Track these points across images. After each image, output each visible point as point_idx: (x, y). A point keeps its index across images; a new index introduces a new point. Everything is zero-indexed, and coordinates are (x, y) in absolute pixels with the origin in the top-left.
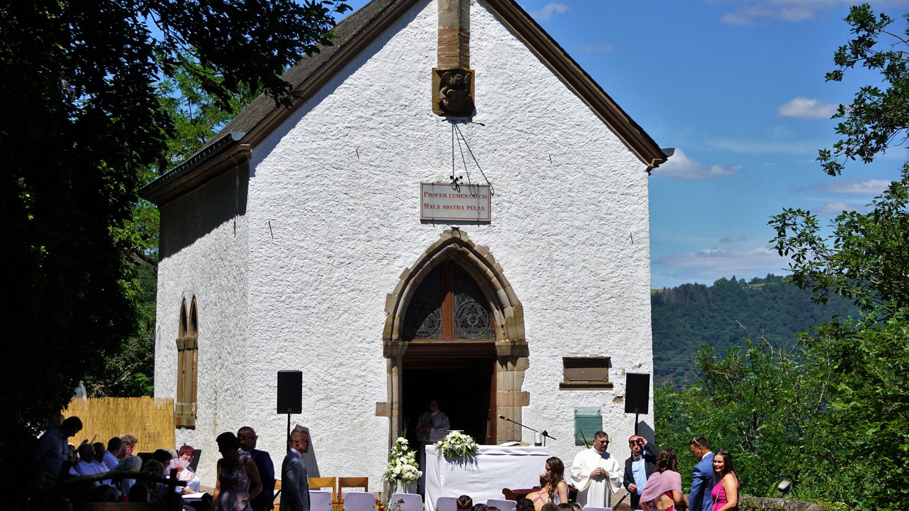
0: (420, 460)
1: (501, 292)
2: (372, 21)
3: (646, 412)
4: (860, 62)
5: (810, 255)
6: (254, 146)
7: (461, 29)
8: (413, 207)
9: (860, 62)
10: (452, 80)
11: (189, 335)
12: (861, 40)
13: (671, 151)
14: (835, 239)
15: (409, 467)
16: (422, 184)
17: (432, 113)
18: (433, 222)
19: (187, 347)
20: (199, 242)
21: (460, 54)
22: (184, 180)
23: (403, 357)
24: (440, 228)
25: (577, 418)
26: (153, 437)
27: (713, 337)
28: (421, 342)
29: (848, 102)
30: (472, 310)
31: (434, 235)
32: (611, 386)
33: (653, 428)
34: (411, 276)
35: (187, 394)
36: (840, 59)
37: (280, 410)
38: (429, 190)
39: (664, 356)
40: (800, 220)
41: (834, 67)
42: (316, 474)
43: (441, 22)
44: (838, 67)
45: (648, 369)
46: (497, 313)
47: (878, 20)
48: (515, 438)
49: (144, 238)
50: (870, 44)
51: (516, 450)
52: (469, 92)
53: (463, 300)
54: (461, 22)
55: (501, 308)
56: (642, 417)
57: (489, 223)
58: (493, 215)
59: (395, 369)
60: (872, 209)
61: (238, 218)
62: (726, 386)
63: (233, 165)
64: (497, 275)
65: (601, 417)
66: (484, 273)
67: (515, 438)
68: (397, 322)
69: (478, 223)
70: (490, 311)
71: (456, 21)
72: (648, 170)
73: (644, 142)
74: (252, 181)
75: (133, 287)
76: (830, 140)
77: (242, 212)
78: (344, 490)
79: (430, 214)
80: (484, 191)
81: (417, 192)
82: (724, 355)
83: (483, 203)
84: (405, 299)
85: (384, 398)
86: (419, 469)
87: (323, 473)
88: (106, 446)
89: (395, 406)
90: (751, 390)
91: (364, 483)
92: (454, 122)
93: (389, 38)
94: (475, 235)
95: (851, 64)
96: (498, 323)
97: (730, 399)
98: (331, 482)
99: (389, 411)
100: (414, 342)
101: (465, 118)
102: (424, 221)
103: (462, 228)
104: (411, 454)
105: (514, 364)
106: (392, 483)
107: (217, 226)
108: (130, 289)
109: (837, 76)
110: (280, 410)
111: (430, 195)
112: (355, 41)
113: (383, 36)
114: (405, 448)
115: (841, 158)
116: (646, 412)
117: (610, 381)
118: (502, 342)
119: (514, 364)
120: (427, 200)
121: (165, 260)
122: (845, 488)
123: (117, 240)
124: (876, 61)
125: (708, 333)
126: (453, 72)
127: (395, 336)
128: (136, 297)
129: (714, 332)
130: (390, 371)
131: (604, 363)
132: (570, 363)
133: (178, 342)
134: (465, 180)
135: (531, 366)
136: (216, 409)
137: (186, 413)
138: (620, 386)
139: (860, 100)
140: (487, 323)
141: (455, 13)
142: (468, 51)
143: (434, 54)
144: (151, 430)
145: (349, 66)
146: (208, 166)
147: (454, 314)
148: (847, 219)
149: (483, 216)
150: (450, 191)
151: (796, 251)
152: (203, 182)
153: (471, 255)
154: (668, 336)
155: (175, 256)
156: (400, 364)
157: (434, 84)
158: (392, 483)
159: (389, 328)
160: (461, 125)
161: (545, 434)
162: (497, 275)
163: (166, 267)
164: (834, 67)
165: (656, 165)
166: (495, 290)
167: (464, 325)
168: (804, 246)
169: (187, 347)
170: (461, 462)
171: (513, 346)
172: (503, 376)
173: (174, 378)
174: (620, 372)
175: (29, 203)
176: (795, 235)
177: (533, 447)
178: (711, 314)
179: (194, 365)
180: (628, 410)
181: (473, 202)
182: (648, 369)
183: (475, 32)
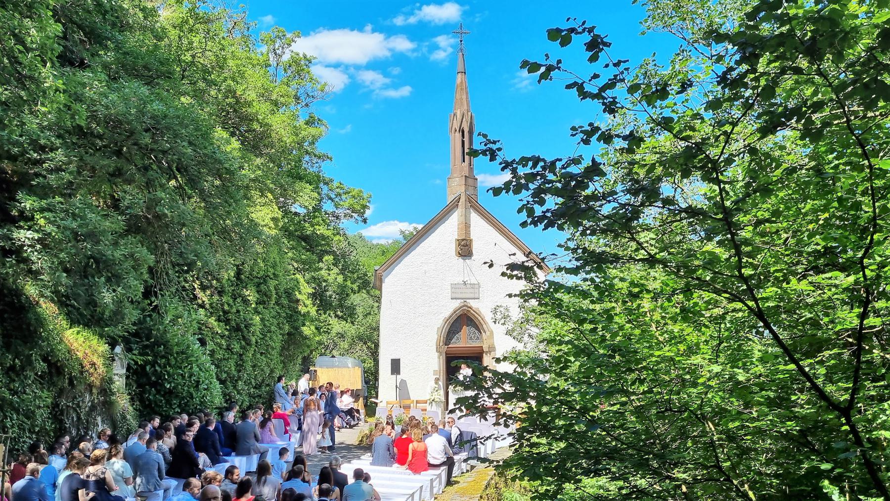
8: (448, 293)
10: (463, 243)
18: (456, 299)
24: (459, 301)
31: (457, 304)
37: (392, 373)
38: (454, 286)
49: (842, 188)
69: (474, 299)
79: (455, 296)
80: (477, 286)
81: (450, 287)
83: (477, 291)
94: (473, 304)
103: (468, 301)
110: (392, 373)
120: (453, 290)
126: (463, 240)
130: (439, 358)
134: (469, 282)
136: (468, 471)
141: (463, 217)
143: (456, 233)
149: (477, 296)
150: (463, 286)
154: (172, 296)
159: (439, 341)
167: (471, 339)
181: (472, 290)
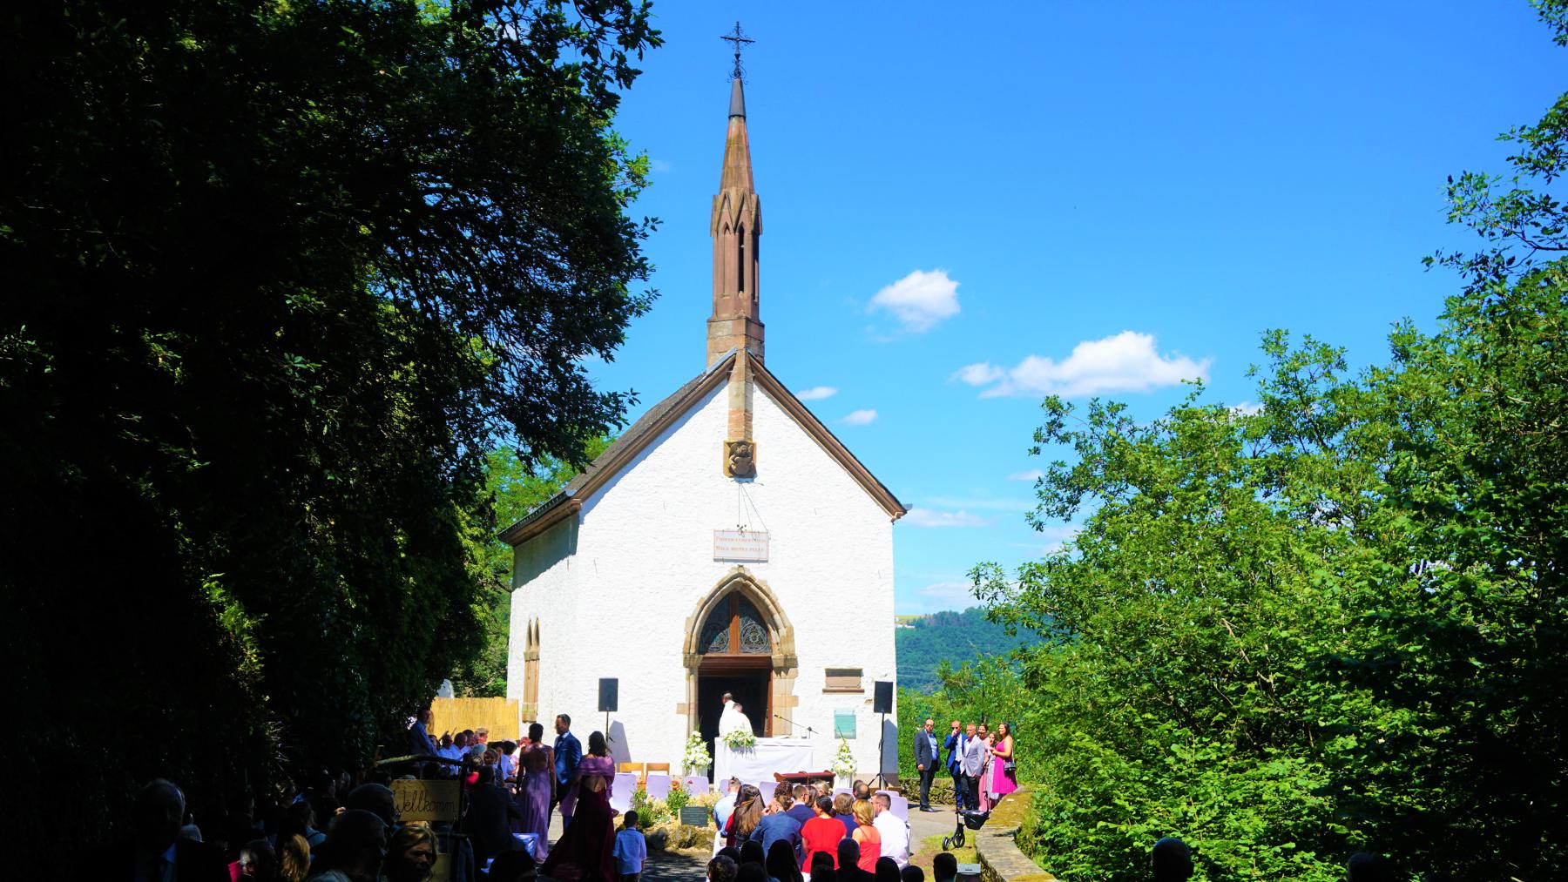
0: (711, 750)
1: (777, 617)
2: (677, 404)
3: (890, 712)
4: (1053, 439)
5: (1001, 597)
6: (583, 500)
7: (746, 411)
9: (1053, 439)
10: (739, 450)
11: (533, 648)
12: (1053, 422)
13: (910, 506)
14: (1019, 584)
15: (702, 755)
16: (715, 531)
17: (723, 475)
18: (723, 560)
19: (532, 658)
20: (542, 576)
21: (745, 430)
22: (531, 527)
23: (699, 668)
24: (729, 565)
25: (836, 716)
26: (503, 730)
27: (964, 653)
28: (713, 655)
29: (1043, 474)
30: (754, 631)
32: (862, 691)
33: (896, 724)
34: (706, 603)
35: (531, 697)
36: (1037, 438)
38: (720, 535)
39: (926, 669)
40: (991, 570)
41: (1033, 444)
42: (628, 759)
43: (730, 406)
44: (1037, 444)
45: (892, 678)
46: (773, 633)
47: (1066, 407)
48: (788, 735)
50: (1061, 426)
51: (786, 742)
52: (752, 459)
53: (747, 622)
54: (746, 405)
55: (777, 629)
56: (887, 716)
57: (767, 561)
58: (770, 556)
59: (692, 677)
60: (1044, 562)
61: (571, 558)
62: (962, 692)
63: (568, 515)
64: (773, 603)
65: (854, 716)
66: (762, 601)
67: (788, 735)
68: (694, 640)
69: (758, 561)
70: (767, 630)
71: (742, 405)
72: (893, 521)
73: (889, 498)
74: (581, 528)
75: (483, 611)
76: (1032, 504)
77: (574, 553)
78: (650, 773)
80: (763, 537)
82: (957, 669)
83: (763, 545)
84: (701, 622)
85: (684, 700)
86: (710, 757)
87: (634, 759)
88: (453, 739)
89: (692, 706)
90: (981, 696)
91: (666, 768)
92: (740, 482)
93: (690, 417)
94: (753, 571)
95: (1046, 441)
96: (774, 641)
97: (964, 703)
98: (640, 767)
99: (687, 710)
100: (707, 655)
101: (749, 480)
102: (716, 560)
103: (745, 565)
104: (704, 744)
105: (787, 673)
106: (688, 768)
107: (555, 563)
108: (480, 611)
109: (1037, 451)
111: (721, 539)
112: (664, 419)
113: (685, 415)
114: (699, 740)
115: (1043, 517)
116: (890, 712)
117: (862, 688)
118: (777, 657)
119: (787, 673)
121: (517, 590)
122: (1050, 773)
123: (471, 573)
124: (1065, 439)
125: (960, 650)
126: (740, 444)
127: (693, 651)
128: (486, 619)
129: (965, 650)
130: (689, 679)
131: (857, 673)
132: (831, 673)
133: (525, 654)
134: (748, 528)
135: (800, 675)
137: (530, 710)
138: (870, 693)
139: (1052, 472)
140: (765, 640)
141: (741, 398)
142: (751, 427)
144: (500, 724)
145: (658, 439)
146: (549, 516)
147: (739, 634)
148: (1027, 569)
150: (737, 536)
151: (990, 595)
152: (545, 529)
153: (753, 587)
155: (524, 587)
156: (696, 673)
157: (725, 452)
158: (688, 768)
159: (689, 644)
160: (745, 485)
161: (810, 729)
162: (773, 603)
163: (518, 595)
164: (1033, 444)
165: (899, 517)
166: (772, 615)
167: (747, 642)
168: (995, 590)
169: (532, 658)
170: (742, 752)
171: (786, 659)
172: (778, 683)
173: (522, 682)
174: (870, 680)
175: (401, 544)
176: (987, 582)
177: (800, 739)
178: (962, 635)
179: (536, 672)
180: (876, 710)
181: (755, 545)
182: (892, 678)
183: (755, 403)
